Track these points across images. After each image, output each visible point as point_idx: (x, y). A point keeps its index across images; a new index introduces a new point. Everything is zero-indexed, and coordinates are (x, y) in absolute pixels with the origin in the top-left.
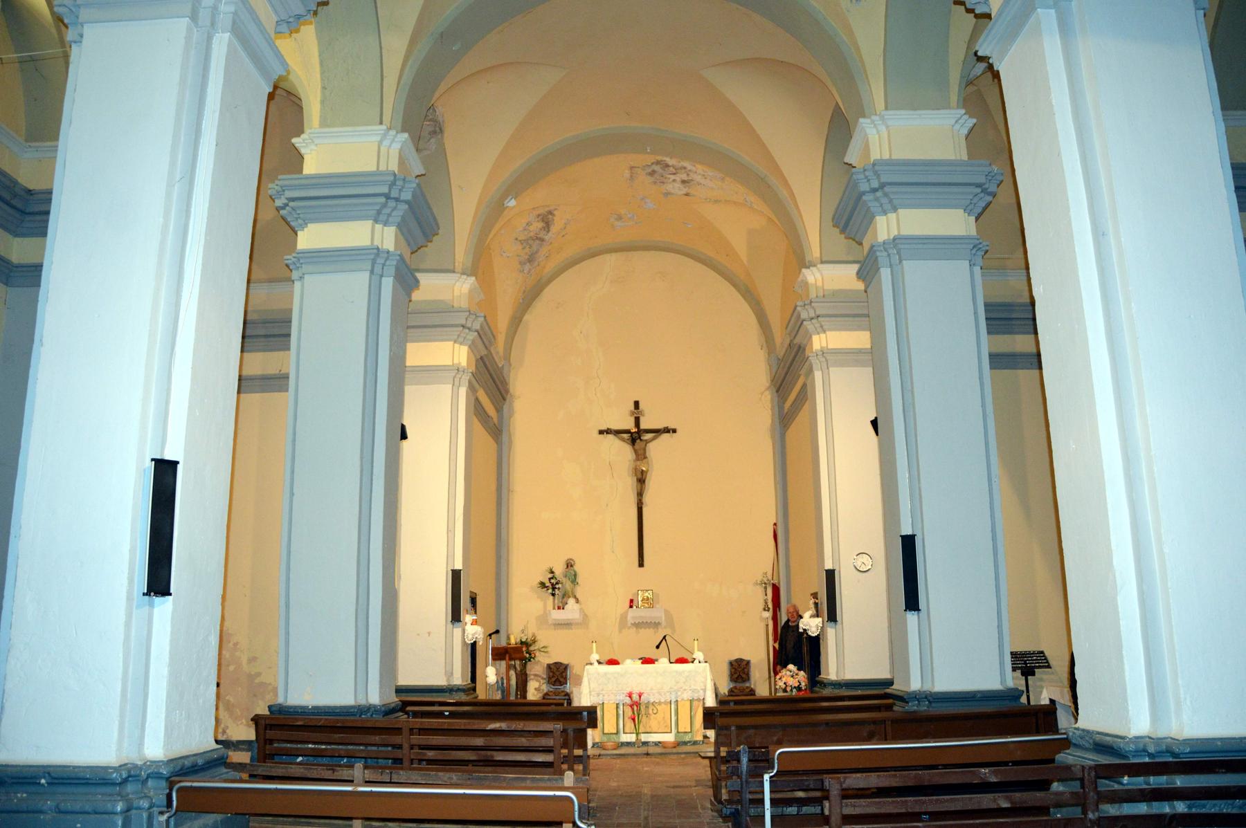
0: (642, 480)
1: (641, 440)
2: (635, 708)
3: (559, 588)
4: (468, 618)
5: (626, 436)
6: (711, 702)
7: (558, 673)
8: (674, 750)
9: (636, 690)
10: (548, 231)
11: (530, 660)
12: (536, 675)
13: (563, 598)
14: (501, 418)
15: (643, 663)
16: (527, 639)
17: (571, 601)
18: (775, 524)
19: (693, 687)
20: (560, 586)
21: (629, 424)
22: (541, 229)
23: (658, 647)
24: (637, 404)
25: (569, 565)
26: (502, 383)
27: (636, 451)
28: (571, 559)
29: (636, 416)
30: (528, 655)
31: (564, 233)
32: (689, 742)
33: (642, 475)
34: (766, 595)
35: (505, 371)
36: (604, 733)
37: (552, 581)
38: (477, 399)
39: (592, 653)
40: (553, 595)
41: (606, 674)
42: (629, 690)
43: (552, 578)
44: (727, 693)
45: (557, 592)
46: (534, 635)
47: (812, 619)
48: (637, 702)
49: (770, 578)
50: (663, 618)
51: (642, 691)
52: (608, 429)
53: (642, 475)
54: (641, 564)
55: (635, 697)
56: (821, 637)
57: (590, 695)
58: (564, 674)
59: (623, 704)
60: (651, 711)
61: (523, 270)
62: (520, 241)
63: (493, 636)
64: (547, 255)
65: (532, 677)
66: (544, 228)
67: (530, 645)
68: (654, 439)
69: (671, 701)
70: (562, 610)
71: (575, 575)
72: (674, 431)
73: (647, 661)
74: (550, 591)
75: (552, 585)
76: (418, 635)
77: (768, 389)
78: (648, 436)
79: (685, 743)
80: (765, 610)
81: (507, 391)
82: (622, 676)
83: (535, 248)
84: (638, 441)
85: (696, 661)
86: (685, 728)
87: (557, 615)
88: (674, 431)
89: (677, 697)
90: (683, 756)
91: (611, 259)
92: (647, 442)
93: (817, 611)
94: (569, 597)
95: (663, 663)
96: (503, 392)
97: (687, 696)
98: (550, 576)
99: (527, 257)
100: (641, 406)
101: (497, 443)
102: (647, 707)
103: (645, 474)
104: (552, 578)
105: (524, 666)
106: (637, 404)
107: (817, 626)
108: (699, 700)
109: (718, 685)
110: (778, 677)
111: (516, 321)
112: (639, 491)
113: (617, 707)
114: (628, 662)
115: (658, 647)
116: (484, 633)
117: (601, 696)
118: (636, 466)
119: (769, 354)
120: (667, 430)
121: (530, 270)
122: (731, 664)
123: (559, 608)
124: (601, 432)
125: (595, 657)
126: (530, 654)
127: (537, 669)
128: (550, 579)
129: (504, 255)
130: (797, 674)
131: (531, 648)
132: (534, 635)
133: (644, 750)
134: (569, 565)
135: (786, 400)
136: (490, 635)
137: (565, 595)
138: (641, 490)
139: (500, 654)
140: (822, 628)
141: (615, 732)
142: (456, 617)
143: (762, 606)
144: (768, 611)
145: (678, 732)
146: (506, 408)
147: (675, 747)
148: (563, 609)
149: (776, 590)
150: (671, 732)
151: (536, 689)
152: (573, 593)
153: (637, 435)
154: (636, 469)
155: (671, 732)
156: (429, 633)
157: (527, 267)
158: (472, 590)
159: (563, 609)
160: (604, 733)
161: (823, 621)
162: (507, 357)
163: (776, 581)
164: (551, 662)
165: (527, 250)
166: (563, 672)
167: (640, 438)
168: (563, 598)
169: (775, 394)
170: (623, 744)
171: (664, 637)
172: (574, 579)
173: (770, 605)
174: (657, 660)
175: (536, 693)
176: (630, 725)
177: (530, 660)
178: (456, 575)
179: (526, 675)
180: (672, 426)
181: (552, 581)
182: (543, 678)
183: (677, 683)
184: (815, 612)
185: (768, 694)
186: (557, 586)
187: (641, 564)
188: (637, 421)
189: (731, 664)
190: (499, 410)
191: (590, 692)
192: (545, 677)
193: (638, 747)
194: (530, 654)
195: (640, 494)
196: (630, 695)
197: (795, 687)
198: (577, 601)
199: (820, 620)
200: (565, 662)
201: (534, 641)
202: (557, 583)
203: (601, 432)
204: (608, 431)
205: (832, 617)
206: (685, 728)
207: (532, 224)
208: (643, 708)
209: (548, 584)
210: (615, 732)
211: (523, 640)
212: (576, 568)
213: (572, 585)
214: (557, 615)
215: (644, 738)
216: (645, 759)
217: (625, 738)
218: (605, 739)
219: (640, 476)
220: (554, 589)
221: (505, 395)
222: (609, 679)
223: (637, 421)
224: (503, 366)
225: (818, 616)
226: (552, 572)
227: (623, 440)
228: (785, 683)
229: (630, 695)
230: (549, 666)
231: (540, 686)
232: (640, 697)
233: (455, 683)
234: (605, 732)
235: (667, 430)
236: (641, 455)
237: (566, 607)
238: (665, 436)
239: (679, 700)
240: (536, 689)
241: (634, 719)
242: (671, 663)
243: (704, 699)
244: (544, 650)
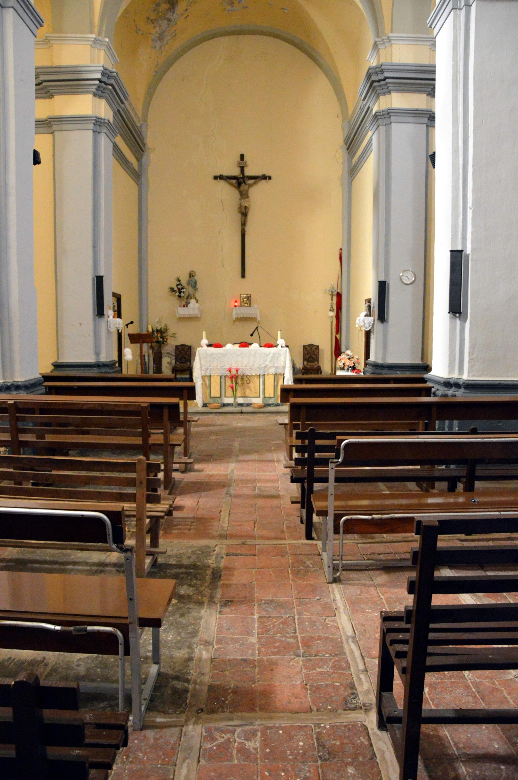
0: (244, 213)
1: (245, 184)
2: (234, 379)
3: (184, 292)
4: (109, 312)
5: (234, 181)
6: (289, 381)
7: (183, 352)
8: (261, 410)
9: (234, 366)
10: (174, 13)
11: (163, 343)
12: (168, 353)
13: (187, 299)
14: (140, 165)
15: (240, 347)
16: (161, 328)
17: (193, 301)
18: (341, 249)
19: (275, 365)
20: (184, 290)
21: (236, 172)
22: (167, 10)
23: (252, 335)
24: (242, 157)
25: (191, 275)
26: (139, 137)
27: (241, 193)
28: (193, 271)
29: (241, 165)
30: (161, 340)
31: (186, 15)
32: (272, 404)
33: (245, 209)
34: (332, 300)
35: (144, 129)
36: (211, 397)
37: (179, 287)
38: (115, 146)
39: (202, 339)
40: (180, 297)
41: (212, 354)
42: (228, 366)
43: (179, 285)
44: (301, 368)
45: (182, 294)
46: (166, 325)
47: (366, 318)
48: (235, 375)
49: (335, 289)
50: (258, 315)
51: (238, 367)
52: (221, 175)
53: (245, 209)
54: (243, 276)
55: (234, 372)
56: (372, 330)
57: (201, 369)
58: (188, 353)
59: (225, 376)
60: (245, 382)
61: (155, 47)
62: (152, 20)
63: (129, 326)
64: (173, 35)
65: (166, 354)
66: (170, 9)
67: (164, 333)
68: (255, 183)
69: (260, 375)
70: (185, 308)
71: (196, 283)
72: (270, 178)
73: (245, 345)
74: (177, 294)
75: (179, 289)
76: (72, 325)
77: (341, 147)
78: (251, 182)
79: (269, 405)
80: (330, 310)
81: (144, 145)
82: (224, 355)
83: (164, 27)
84: (243, 184)
85: (279, 347)
86: (270, 394)
87: (183, 312)
88: (270, 178)
89: (264, 371)
90: (267, 414)
91: (226, 40)
92: (250, 186)
93: (370, 312)
94: (191, 298)
95: (255, 346)
96: (142, 146)
97: (272, 371)
98: (178, 283)
99: (157, 35)
100: (246, 158)
101: (138, 185)
102: (242, 379)
103: (247, 209)
104: (179, 285)
105: (160, 347)
106: (242, 157)
107: (370, 323)
108: (280, 374)
109: (295, 362)
110: (339, 359)
111: (151, 90)
112: (243, 222)
113: (221, 378)
114: (229, 346)
115: (252, 335)
116: (123, 323)
117: (209, 370)
118: (241, 203)
119: (343, 121)
120: (264, 177)
121: (161, 47)
122: (305, 347)
123: (184, 306)
124: (216, 178)
125: (204, 341)
126: (163, 339)
127: (169, 348)
128: (177, 285)
129: (140, 32)
130: (352, 358)
131: (165, 335)
132: (166, 325)
133: (239, 409)
134: (191, 275)
135: (354, 155)
136: (127, 325)
137: (189, 297)
138: (245, 221)
139: (135, 338)
140: (373, 325)
141: (219, 396)
142: (100, 311)
143: (329, 307)
144: (333, 311)
145: (265, 397)
146: (144, 159)
147: (262, 408)
148: (187, 307)
149: (339, 296)
150: (259, 397)
151: (168, 363)
152: (194, 295)
153: (242, 180)
154: (241, 205)
155: (259, 397)
156: (81, 324)
157: (158, 44)
158: (115, 292)
159: (187, 307)
160: (211, 397)
161: (374, 320)
162: (145, 120)
163: (339, 291)
164: (179, 344)
165: (157, 29)
166: (187, 351)
167: (244, 182)
168: (187, 299)
169: (345, 151)
170: (225, 405)
171: (257, 328)
172: (195, 286)
173: (335, 307)
174: (251, 344)
175: (168, 365)
176: (229, 392)
177: (163, 343)
178: (99, 281)
179: (161, 353)
180: (267, 174)
181: (179, 287)
182: (173, 355)
183: (264, 361)
184: (368, 313)
185: (330, 372)
186: (182, 291)
187: (243, 276)
188: (242, 169)
189: (305, 347)
190: (139, 159)
191: (201, 367)
192: (174, 354)
193: (235, 407)
194: (163, 339)
195: (244, 224)
196: (230, 371)
197: (351, 367)
198: (197, 301)
199: (371, 319)
200: (189, 344)
201: (166, 330)
202: (183, 288)
203: (216, 178)
204: (221, 177)
205: (382, 317)
206: (270, 394)
207: (160, 5)
208: (239, 381)
209: (176, 289)
210: (219, 396)
211: (159, 329)
212: (196, 278)
213: (193, 290)
214: (183, 312)
215: (240, 400)
216: (239, 416)
217: (229, 400)
218: (211, 401)
219: (243, 210)
220: (180, 292)
221: (143, 148)
222: (215, 358)
223: (242, 169)
224: (142, 124)
225: (370, 316)
226: (179, 281)
227: (232, 184)
228: (344, 364)
229: (230, 371)
230: (177, 347)
231: (171, 361)
232: (237, 371)
233: (101, 360)
234: (212, 395)
235: (264, 177)
236: (244, 195)
237: (189, 305)
238: (263, 182)
239: (266, 374)
240: (168, 363)
241: (232, 388)
242: (261, 347)
243: (284, 374)
244: (174, 335)
